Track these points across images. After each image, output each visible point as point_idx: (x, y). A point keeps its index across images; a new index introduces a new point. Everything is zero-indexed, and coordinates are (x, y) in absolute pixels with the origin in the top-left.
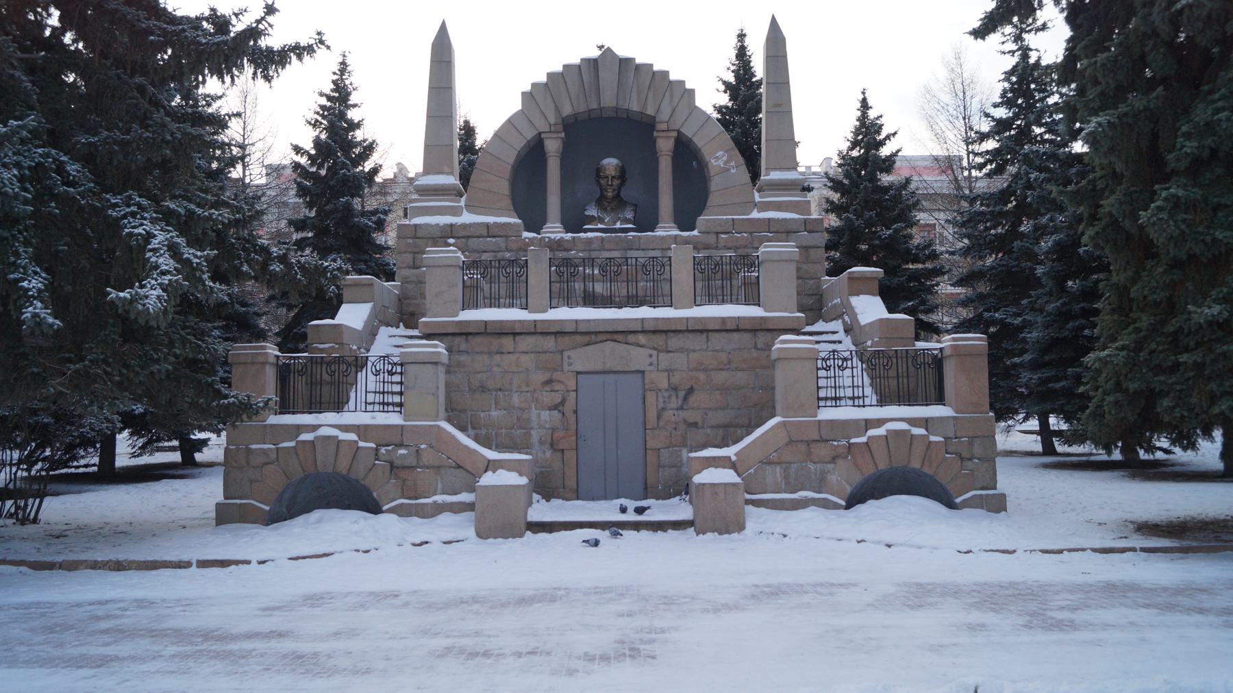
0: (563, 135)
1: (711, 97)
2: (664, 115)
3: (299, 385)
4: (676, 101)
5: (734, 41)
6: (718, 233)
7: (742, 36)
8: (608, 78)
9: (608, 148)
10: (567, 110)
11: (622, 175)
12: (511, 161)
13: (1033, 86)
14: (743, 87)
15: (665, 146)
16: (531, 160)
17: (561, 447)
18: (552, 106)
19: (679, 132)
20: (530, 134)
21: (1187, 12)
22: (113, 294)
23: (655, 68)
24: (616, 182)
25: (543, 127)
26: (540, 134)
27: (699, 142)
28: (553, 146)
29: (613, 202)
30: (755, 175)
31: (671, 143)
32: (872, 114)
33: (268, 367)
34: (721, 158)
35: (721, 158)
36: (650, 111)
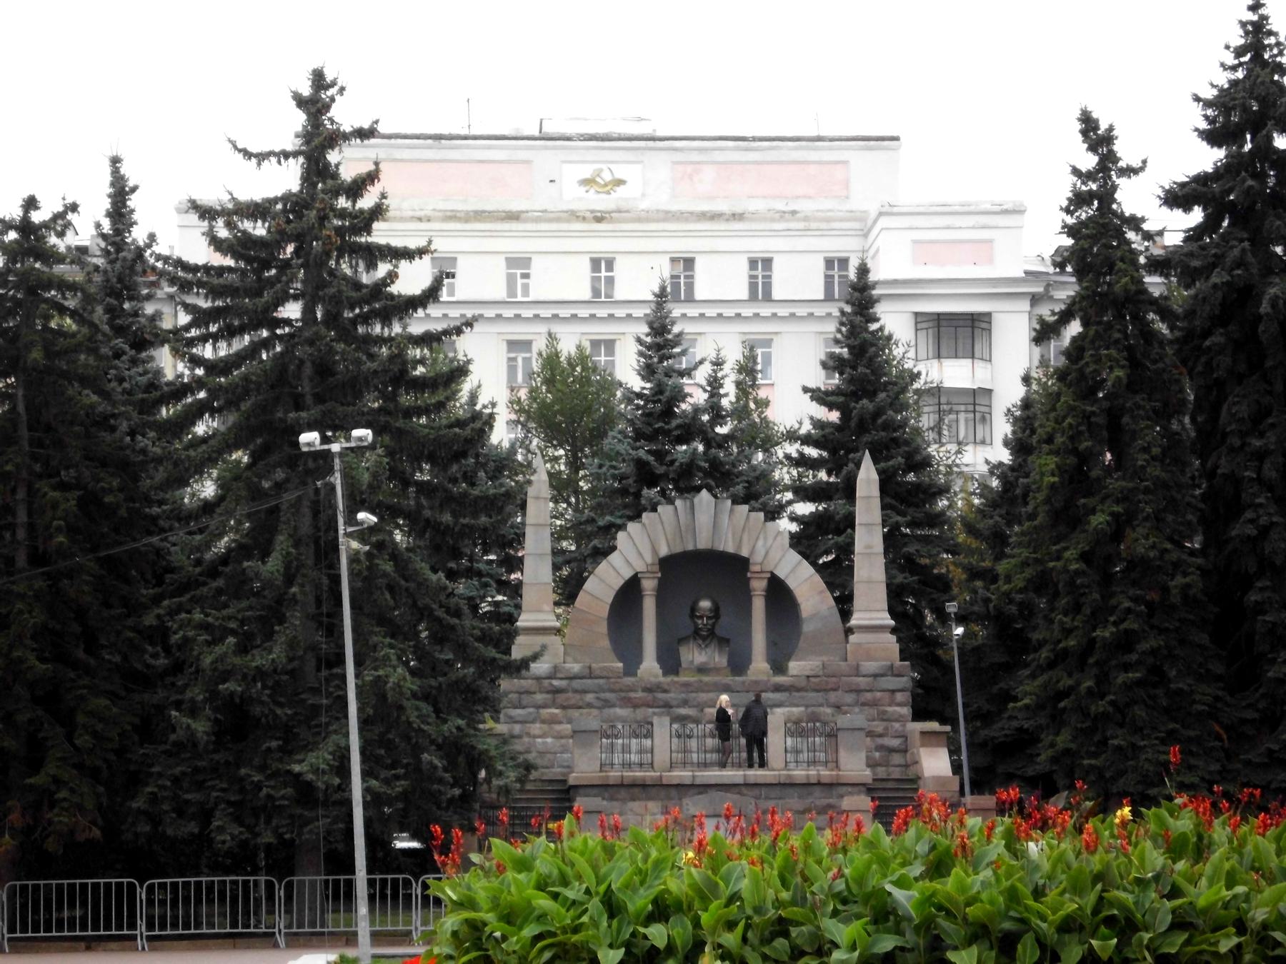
2: (757, 558)
4: (770, 542)
5: (107, 170)
6: (893, 691)
7: (115, 161)
10: (664, 551)
11: (716, 612)
12: (610, 600)
15: (759, 586)
19: (772, 573)
20: (628, 574)
22: (415, 845)
25: (640, 567)
27: (792, 583)
28: (649, 585)
29: (708, 635)
30: (845, 614)
31: (764, 584)
32: (138, 235)
36: (745, 553)
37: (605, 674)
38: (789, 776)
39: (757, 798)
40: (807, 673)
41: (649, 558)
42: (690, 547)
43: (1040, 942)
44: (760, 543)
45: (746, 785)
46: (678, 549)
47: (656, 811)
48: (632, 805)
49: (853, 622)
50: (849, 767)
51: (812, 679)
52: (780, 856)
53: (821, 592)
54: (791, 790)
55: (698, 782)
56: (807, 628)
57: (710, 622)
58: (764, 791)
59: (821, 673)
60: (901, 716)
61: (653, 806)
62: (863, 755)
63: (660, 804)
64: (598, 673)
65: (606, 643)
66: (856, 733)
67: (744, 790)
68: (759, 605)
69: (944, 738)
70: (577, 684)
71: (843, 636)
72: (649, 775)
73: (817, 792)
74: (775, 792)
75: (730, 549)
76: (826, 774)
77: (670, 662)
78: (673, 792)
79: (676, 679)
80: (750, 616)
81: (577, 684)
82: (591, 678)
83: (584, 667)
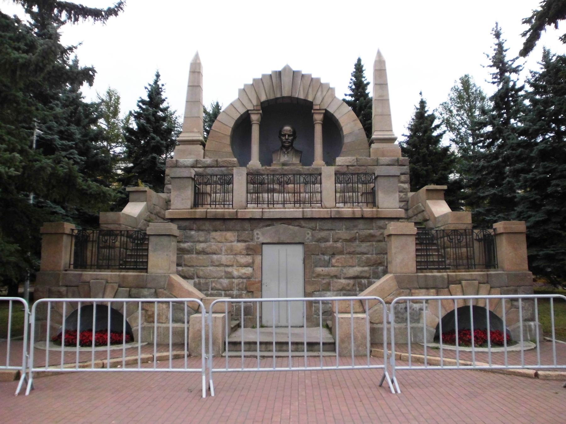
0: (261, 112)
1: (343, 90)
2: (318, 101)
3: (90, 252)
4: (324, 93)
8: (286, 81)
9: (285, 118)
10: (263, 98)
11: (294, 134)
13: (511, 99)
14: (359, 86)
15: (318, 117)
16: (243, 125)
17: (252, 290)
18: (255, 96)
19: (326, 110)
20: (242, 111)
21: (362, 265)
23: (313, 76)
24: (291, 138)
25: (250, 107)
26: (248, 111)
27: (337, 115)
28: (255, 118)
29: (287, 147)
33: (65, 237)
34: (349, 122)
35: (349, 122)
36: (310, 99)
37: (225, 164)
38: (338, 212)
39: (313, 229)
40: (347, 164)
41: (255, 103)
42: (279, 96)
43: (117, 193)
44: (319, 93)
45: (304, 219)
46: (272, 97)
47: (233, 239)
48: (214, 234)
49: (373, 137)
50: (385, 206)
51: (350, 167)
52: (31, 164)
53: (354, 121)
54: (338, 224)
55: (266, 216)
56: (347, 140)
57: (291, 138)
58: (318, 224)
59: (355, 164)
60: (404, 189)
61: (230, 235)
62: (397, 196)
63: (236, 234)
64: (221, 164)
65: (229, 149)
66: (391, 179)
67: (303, 223)
68: (318, 130)
69: (442, 195)
70: (209, 171)
71: (367, 145)
72: (227, 211)
73: (361, 224)
74: (328, 225)
75: (302, 97)
76: (368, 211)
77: (266, 160)
78: (247, 225)
79: (268, 168)
80: (314, 144)
81: (209, 171)
82: (217, 167)
83: (213, 161)
